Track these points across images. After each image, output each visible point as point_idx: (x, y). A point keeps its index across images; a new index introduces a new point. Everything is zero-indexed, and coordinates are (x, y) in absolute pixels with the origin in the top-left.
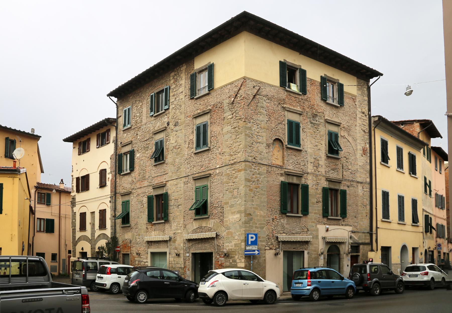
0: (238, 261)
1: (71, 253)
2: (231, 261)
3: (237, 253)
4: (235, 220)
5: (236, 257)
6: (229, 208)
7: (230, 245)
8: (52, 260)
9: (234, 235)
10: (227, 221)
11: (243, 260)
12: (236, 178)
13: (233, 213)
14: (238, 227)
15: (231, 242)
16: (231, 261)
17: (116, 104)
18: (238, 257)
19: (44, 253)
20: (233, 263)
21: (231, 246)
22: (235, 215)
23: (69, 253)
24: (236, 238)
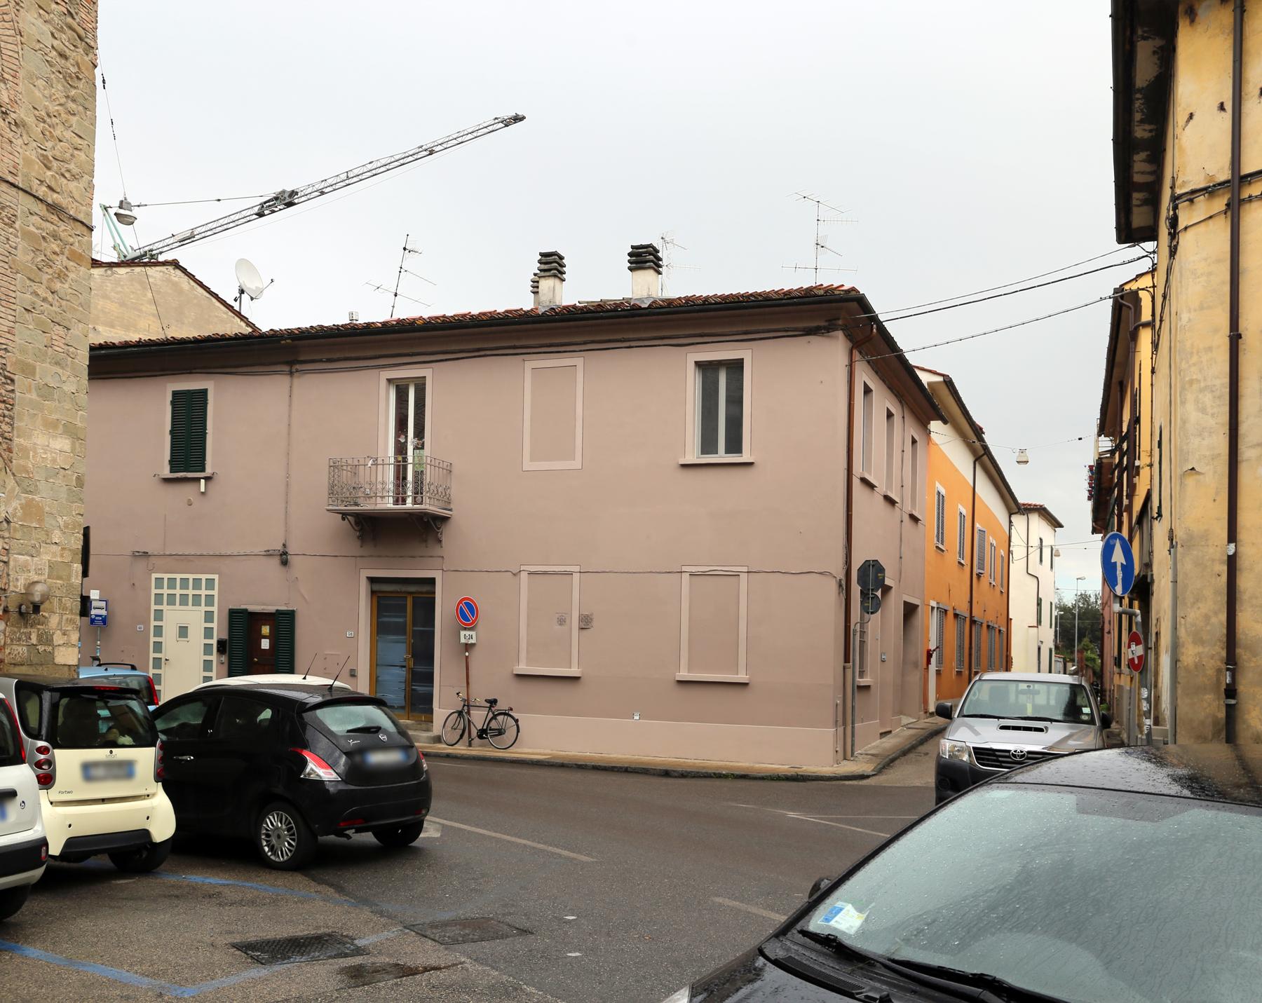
0: (58, 639)
1: (212, 622)
2: (34, 640)
3: (56, 601)
4: (54, 460)
5: (54, 621)
6: (34, 396)
7: (33, 562)
8: (175, 464)
9: (49, 522)
10: (25, 451)
11: (75, 637)
12: (61, 276)
13: (51, 425)
14: (63, 495)
15: (39, 554)
16: (34, 640)
17: (1015, 507)
18: (60, 623)
19: (293, 612)
20: (41, 648)
21: (39, 571)
22: (54, 437)
23: (205, 670)
24: (57, 536)
